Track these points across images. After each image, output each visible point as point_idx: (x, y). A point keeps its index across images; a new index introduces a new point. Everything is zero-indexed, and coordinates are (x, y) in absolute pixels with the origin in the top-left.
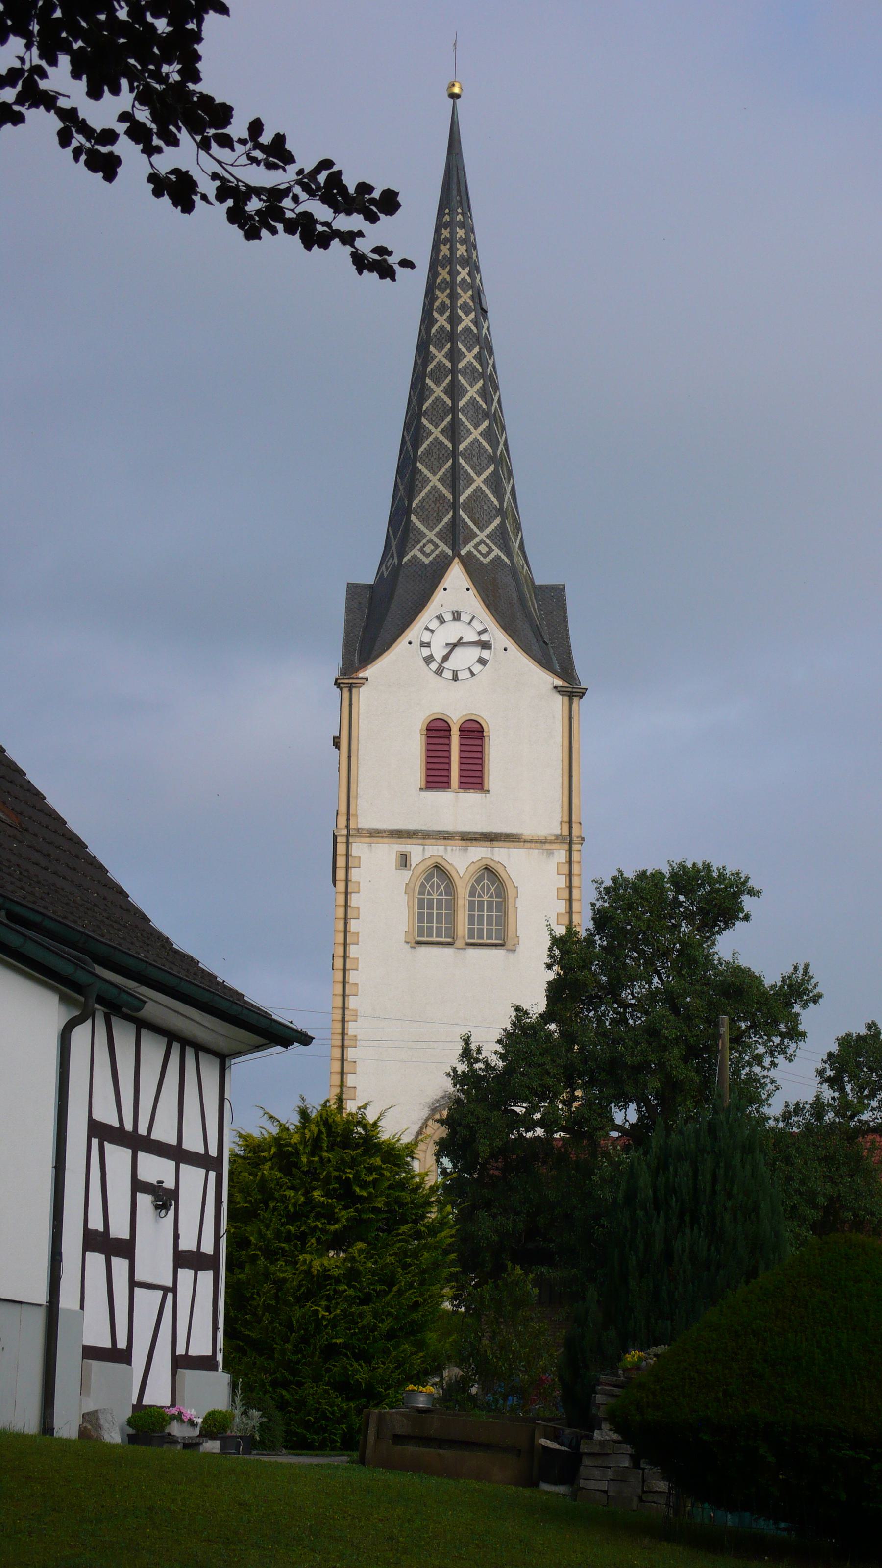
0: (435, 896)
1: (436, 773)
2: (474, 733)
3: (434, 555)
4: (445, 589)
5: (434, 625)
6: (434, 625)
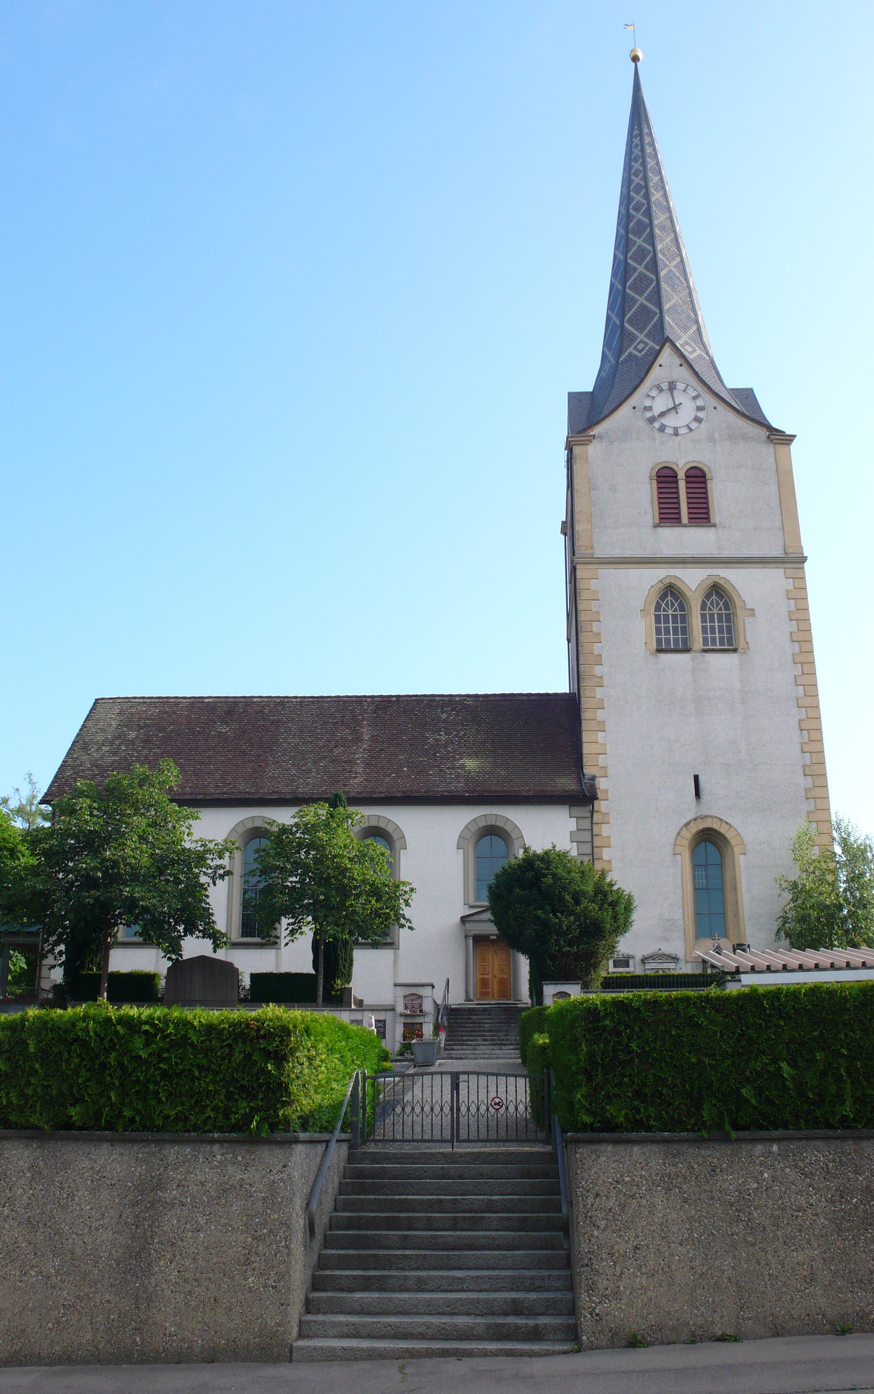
0: (670, 612)
1: (696, 511)
2: (698, 478)
3: (645, 351)
4: (660, 366)
5: (654, 393)
6: (654, 393)
